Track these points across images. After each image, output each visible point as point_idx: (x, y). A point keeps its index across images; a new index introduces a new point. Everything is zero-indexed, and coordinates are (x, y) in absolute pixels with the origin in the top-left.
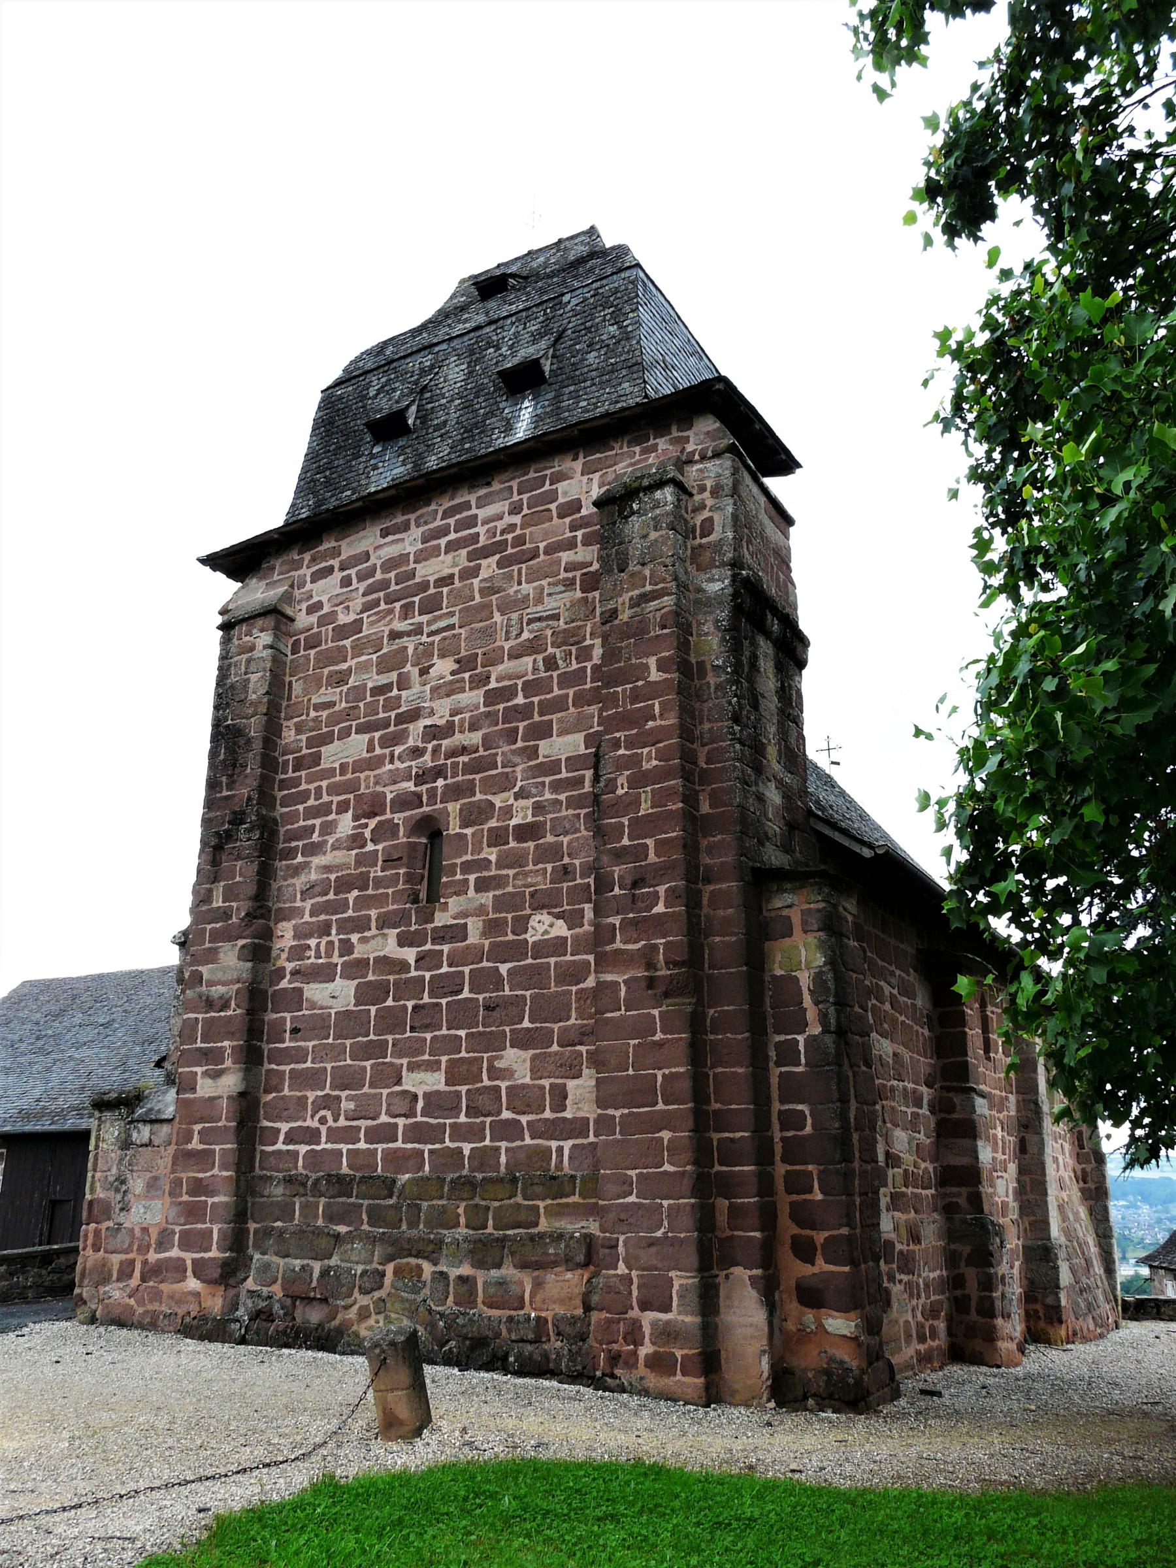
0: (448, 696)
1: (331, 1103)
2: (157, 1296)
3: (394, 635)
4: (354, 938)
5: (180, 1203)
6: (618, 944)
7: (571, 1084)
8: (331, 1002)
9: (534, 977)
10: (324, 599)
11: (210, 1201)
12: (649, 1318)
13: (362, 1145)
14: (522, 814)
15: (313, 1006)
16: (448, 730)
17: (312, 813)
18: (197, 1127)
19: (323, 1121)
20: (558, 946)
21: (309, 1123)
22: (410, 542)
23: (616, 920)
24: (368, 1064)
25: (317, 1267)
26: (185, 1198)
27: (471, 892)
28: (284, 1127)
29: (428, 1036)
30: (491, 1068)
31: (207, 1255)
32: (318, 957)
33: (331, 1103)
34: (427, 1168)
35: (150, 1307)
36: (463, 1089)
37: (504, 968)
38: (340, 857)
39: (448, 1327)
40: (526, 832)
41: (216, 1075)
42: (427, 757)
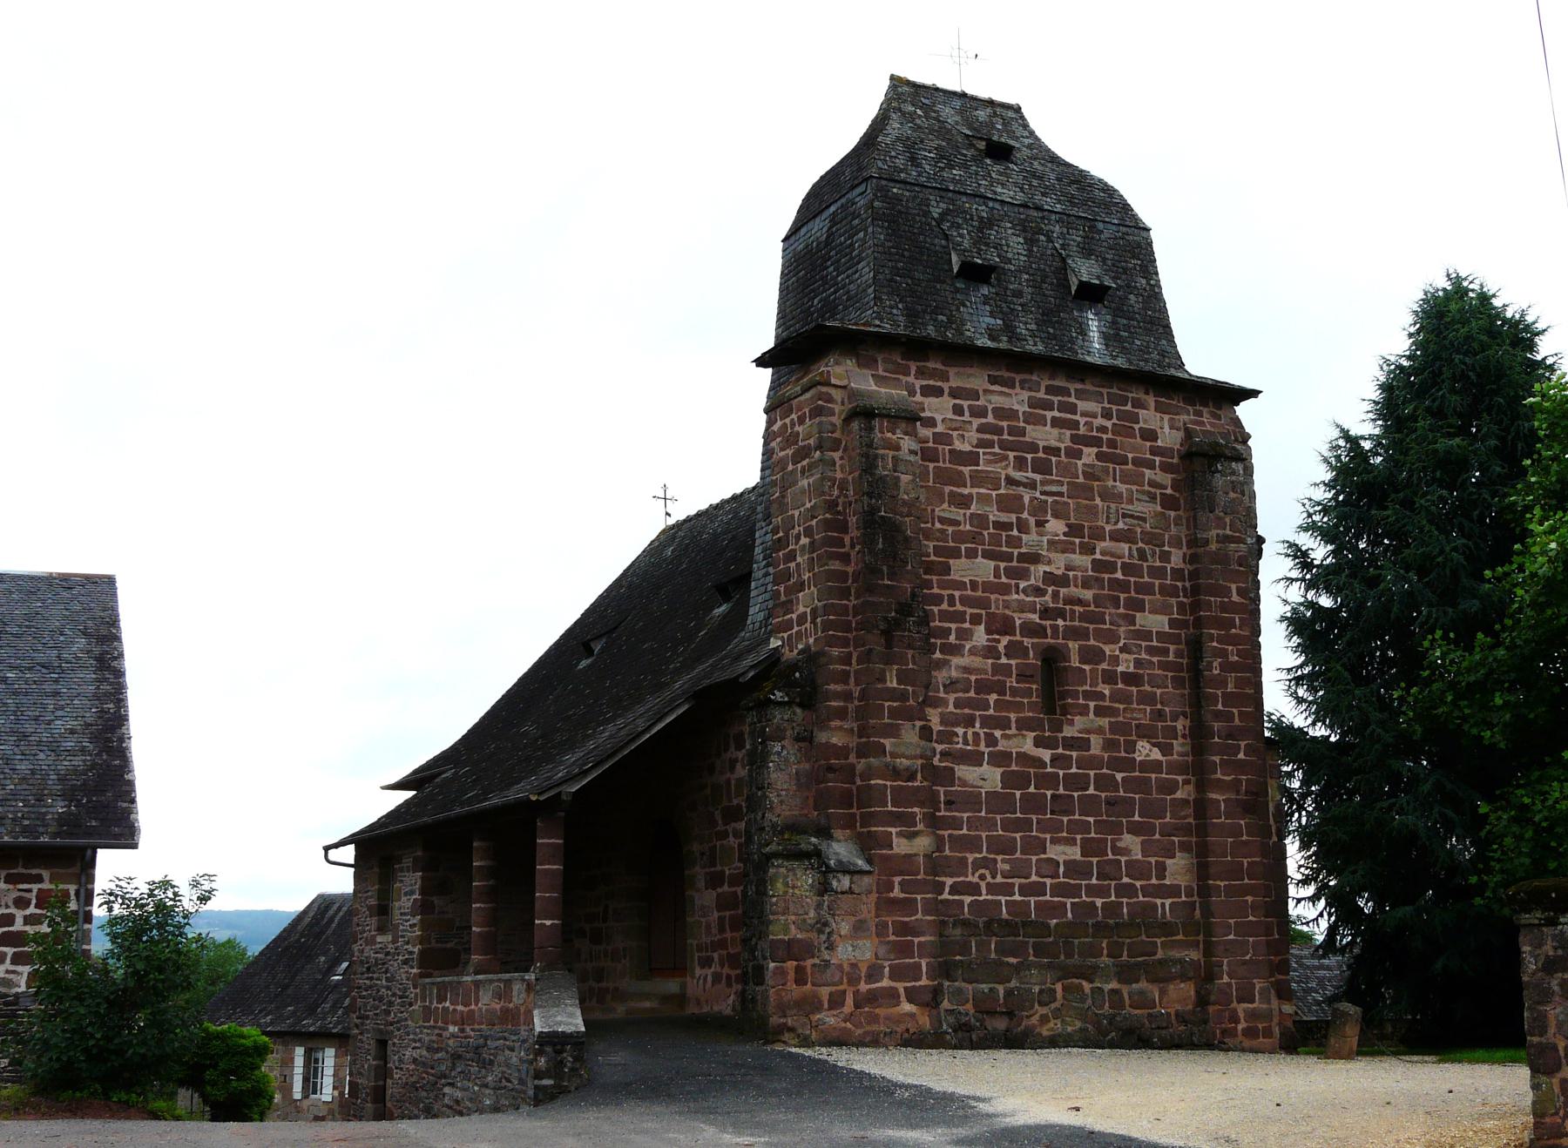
0: (1063, 552)
2: (874, 1019)
3: (1011, 481)
4: (998, 733)
6: (1219, 776)
7: (1169, 862)
8: (981, 783)
9: (1141, 785)
10: (939, 418)
11: (916, 940)
12: (1242, 1008)
13: (1017, 897)
14: (1126, 665)
15: (964, 783)
16: (1062, 581)
17: (945, 616)
18: (897, 879)
19: (982, 877)
20: (1155, 766)
21: (970, 878)
22: (1018, 400)
23: (1217, 759)
24: (1018, 836)
25: (1001, 989)
26: (892, 938)
27: (1091, 715)
28: (949, 881)
29: (1065, 819)
30: (1114, 847)
32: (966, 742)
33: (989, 864)
35: (868, 1028)
36: (1095, 860)
37: (1119, 776)
38: (977, 662)
39: (1110, 1023)
40: (1130, 679)
41: (911, 836)
42: (1048, 598)
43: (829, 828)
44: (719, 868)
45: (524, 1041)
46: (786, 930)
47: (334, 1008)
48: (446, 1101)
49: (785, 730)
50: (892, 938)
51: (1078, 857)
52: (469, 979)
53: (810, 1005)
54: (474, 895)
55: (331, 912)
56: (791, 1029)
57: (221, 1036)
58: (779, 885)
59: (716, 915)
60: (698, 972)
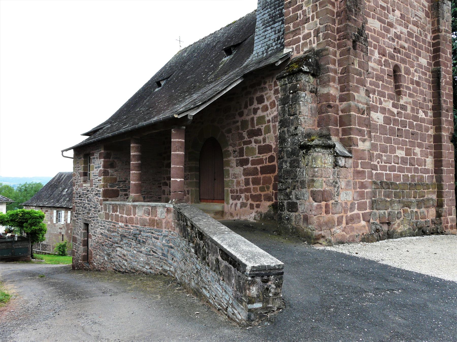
1: (380, 156)
2: (352, 229)
5: (357, 192)
7: (427, 159)
11: (366, 191)
19: (378, 163)
26: (358, 190)
31: (366, 211)
33: (380, 156)
34: (402, 180)
41: (364, 141)
43: (329, 135)
44: (245, 157)
45: (165, 236)
46: (322, 186)
47: (64, 200)
48: (118, 253)
49: (306, 86)
50: (358, 190)
51: (404, 156)
52: (130, 204)
53: (329, 224)
54: (131, 167)
55: (62, 177)
56: (323, 237)
57: (28, 213)
58: (319, 162)
59: (243, 177)
60: (231, 201)
